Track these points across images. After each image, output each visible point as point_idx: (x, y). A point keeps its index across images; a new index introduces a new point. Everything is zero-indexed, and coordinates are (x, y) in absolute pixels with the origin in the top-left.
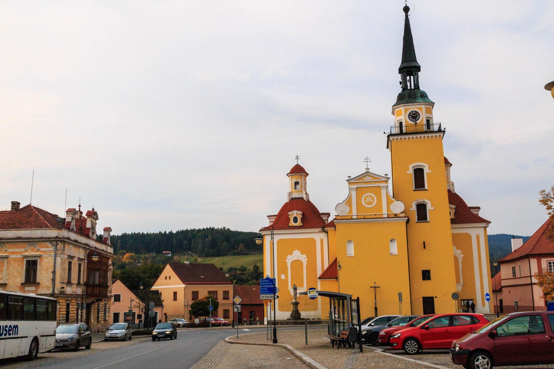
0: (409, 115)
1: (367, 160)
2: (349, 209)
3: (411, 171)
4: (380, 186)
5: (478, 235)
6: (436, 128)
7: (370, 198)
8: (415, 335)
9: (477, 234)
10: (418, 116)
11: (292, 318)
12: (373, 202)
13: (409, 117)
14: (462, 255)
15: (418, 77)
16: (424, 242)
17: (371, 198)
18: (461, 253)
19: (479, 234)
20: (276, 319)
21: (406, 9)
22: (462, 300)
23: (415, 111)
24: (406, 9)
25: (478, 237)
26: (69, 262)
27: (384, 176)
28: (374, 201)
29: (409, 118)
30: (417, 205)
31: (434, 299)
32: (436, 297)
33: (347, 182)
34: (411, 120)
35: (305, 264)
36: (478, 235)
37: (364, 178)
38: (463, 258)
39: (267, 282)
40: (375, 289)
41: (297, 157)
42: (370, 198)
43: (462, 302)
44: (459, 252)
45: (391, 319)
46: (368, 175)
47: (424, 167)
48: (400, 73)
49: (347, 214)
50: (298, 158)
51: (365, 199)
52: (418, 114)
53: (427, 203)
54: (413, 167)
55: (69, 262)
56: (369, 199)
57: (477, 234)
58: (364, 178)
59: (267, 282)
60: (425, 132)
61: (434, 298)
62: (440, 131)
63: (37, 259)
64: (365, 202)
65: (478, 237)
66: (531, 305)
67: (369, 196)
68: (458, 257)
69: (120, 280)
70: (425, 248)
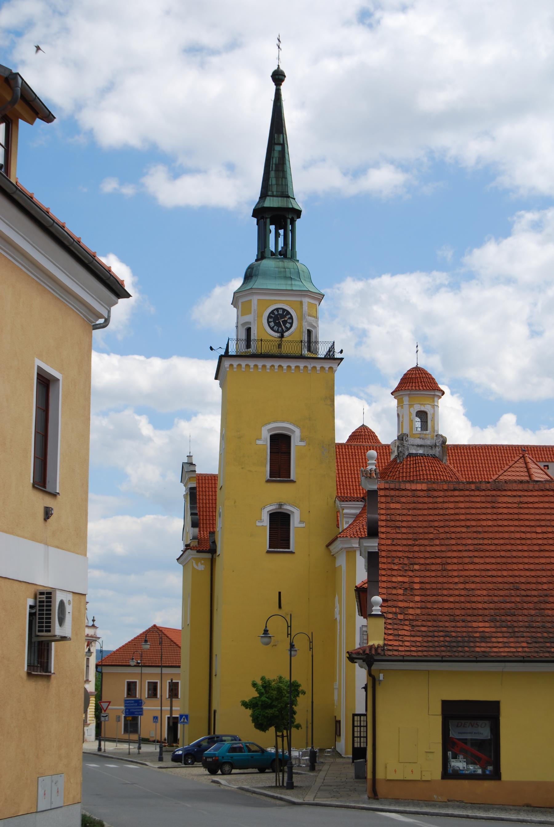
0: (269, 317)
3: (265, 441)
6: (322, 351)
10: (276, 313)
13: (270, 320)
15: (293, 231)
16: (280, 593)
20: (274, 784)
23: (284, 310)
26: (87, 658)
29: (269, 322)
30: (270, 514)
31: (357, 673)
34: (272, 329)
39: (132, 703)
45: (207, 740)
47: (293, 432)
48: (254, 215)
52: (288, 317)
53: (293, 512)
54: (269, 430)
55: (87, 658)
59: (132, 703)
60: (302, 357)
62: (330, 357)
63: (256, 263)
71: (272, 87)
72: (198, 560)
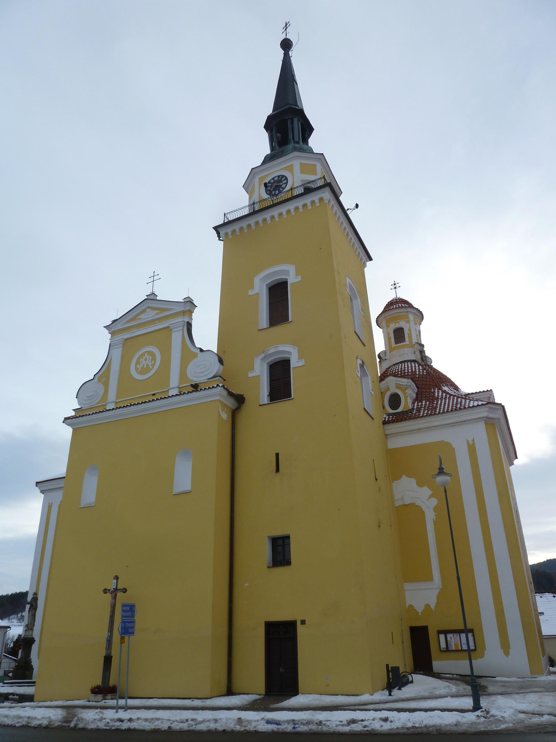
1: (154, 278)
2: (103, 391)
4: (168, 327)
5: (471, 442)
7: (147, 357)
8: (394, 732)
9: (468, 441)
11: (390, 669)
12: (153, 365)
14: (434, 502)
16: (277, 455)
17: (151, 357)
18: (431, 496)
19: (473, 440)
21: (286, 45)
22: (440, 632)
23: (279, 176)
24: (286, 45)
25: (472, 449)
27: (183, 301)
28: (155, 362)
32: (303, 622)
33: (106, 331)
35: (430, 516)
36: (471, 442)
37: (140, 317)
38: (435, 509)
40: (115, 597)
41: (395, 284)
42: (147, 357)
43: (442, 637)
44: (426, 491)
46: (149, 307)
49: (98, 403)
50: (397, 285)
51: (138, 362)
56: (146, 360)
57: (468, 441)
58: (142, 316)
61: (299, 623)
64: (137, 369)
65: (472, 449)
66: (435, 662)
67: (146, 354)
68: (424, 508)
69: (464, 629)
70: (278, 470)
71: (281, 53)
72: (224, 405)
